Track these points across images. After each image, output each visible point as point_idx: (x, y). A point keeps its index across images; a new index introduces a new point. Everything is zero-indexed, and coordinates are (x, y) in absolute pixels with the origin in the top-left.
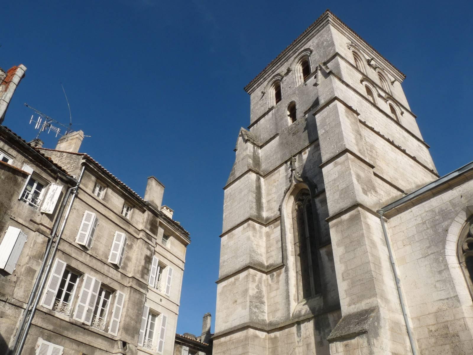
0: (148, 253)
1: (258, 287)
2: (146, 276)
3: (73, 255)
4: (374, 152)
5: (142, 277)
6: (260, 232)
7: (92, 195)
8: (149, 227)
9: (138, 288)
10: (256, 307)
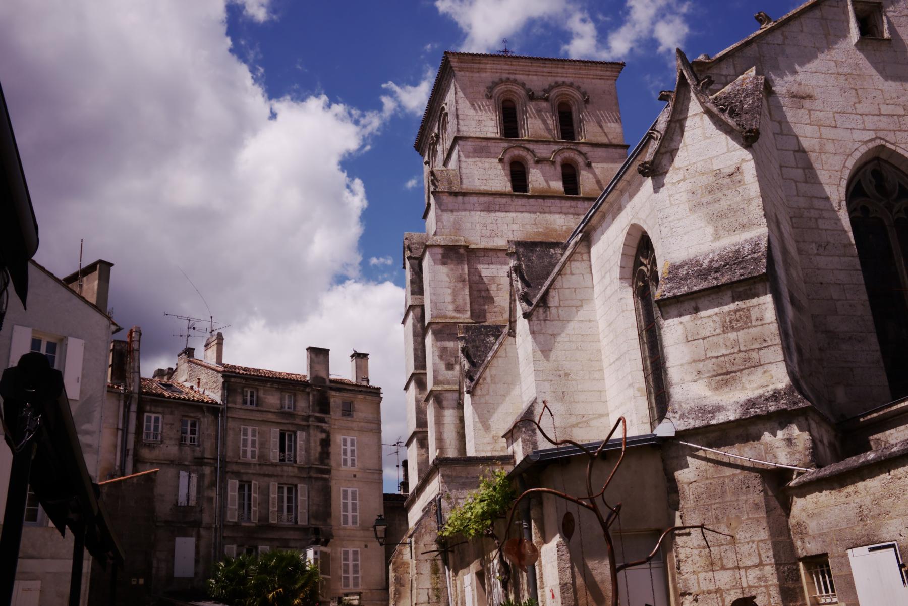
0: (324, 436)
2: (326, 461)
3: (242, 471)
5: (322, 463)
7: (244, 407)
8: (317, 408)
9: (320, 476)
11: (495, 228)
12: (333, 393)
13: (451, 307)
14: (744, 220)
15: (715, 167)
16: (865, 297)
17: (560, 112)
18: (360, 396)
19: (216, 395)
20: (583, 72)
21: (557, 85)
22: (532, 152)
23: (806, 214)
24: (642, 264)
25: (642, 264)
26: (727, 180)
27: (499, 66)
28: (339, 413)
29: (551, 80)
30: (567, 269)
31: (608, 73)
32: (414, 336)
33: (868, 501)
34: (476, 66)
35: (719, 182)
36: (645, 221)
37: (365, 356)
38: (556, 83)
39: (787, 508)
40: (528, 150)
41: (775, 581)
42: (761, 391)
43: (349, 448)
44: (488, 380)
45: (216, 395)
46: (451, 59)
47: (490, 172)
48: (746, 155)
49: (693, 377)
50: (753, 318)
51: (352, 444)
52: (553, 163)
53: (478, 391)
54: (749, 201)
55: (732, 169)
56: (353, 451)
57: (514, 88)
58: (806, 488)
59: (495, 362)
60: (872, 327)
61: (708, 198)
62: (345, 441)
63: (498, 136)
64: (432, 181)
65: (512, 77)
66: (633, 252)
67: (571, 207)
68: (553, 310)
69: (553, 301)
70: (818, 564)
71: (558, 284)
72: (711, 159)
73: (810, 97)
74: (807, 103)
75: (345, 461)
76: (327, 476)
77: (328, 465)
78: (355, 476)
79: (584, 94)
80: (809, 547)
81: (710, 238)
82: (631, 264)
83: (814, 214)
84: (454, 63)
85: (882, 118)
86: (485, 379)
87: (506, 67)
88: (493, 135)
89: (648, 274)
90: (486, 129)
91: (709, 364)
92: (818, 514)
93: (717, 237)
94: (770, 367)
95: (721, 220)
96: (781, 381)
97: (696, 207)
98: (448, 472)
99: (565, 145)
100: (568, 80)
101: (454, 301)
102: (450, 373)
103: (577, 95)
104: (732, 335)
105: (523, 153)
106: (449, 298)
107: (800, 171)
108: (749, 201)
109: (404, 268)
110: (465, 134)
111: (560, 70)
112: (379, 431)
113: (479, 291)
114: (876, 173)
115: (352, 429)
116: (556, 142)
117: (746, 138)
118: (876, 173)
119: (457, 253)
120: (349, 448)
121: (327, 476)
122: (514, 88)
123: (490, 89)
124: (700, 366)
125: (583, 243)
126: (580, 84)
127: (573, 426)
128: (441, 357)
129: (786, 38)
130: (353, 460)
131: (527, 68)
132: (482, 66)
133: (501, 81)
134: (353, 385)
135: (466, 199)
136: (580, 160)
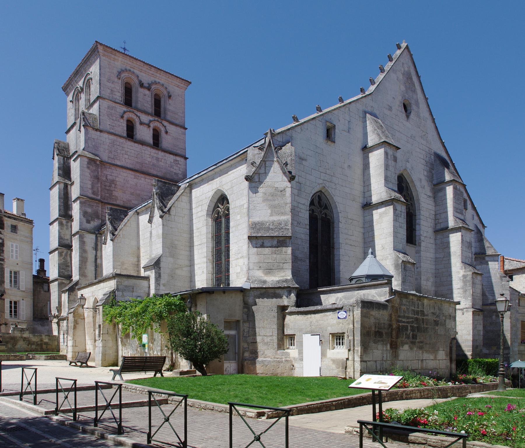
1: (64, 258)
4: (113, 185)
6: (67, 225)
10: (63, 269)
11: (116, 154)
12: (6, 219)
13: (90, 191)
14: (283, 211)
15: (276, 186)
16: (308, 245)
17: (155, 99)
18: (21, 223)
19: (257, 300)
20: (170, 80)
21: (156, 83)
22: (139, 117)
23: (296, 209)
24: (218, 207)
25: (218, 207)
26: (279, 193)
27: (126, 61)
28: (10, 230)
29: (152, 79)
30: (180, 199)
31: (182, 85)
32: (59, 198)
33: (314, 321)
34: (113, 56)
35: (276, 192)
36: (226, 190)
37: (22, 200)
38: (155, 82)
39: (284, 319)
40: (137, 116)
41: (276, 341)
42: (282, 278)
43: (14, 249)
44: (121, 236)
45: (257, 300)
46: (99, 46)
47: (116, 122)
48: (289, 185)
49: (258, 268)
50: (283, 251)
51: (16, 248)
52: (149, 126)
53: (116, 240)
54: (287, 204)
55: (282, 189)
56: (16, 251)
57: (133, 77)
58: (291, 313)
59: (125, 228)
60: (308, 257)
61: (270, 198)
62: (12, 246)
63: (122, 103)
64: (83, 118)
65: (132, 70)
66: (216, 201)
67: (155, 153)
68: (173, 217)
69: (173, 212)
70: (292, 337)
71: (175, 205)
72: (275, 182)
73: (306, 160)
74: (304, 162)
75: (12, 255)
76: (2, 262)
77: (3, 256)
78: (17, 264)
79: (169, 93)
80: (287, 332)
81: (269, 215)
82: (213, 206)
83: (299, 210)
84: (100, 48)
85: (327, 175)
86: (119, 235)
87: (129, 63)
88: (119, 101)
89: (222, 213)
90: (115, 97)
91: (265, 264)
92: (293, 322)
93: (271, 215)
94: (286, 270)
95: (275, 209)
96: (289, 276)
97: (264, 201)
98: (120, 280)
99: (156, 119)
100: (162, 82)
101: (92, 188)
102: (89, 225)
103: (165, 93)
104: (275, 256)
105: (135, 117)
106: (90, 186)
107: (297, 191)
108: (287, 204)
109: (53, 159)
110: (104, 96)
111: (158, 75)
112: (32, 243)
113: (105, 186)
114: (319, 197)
115: (16, 240)
116: (152, 115)
117: (291, 178)
118: (319, 197)
119: (95, 163)
120: (14, 249)
121: (2, 262)
122: (133, 77)
123: (120, 73)
124: (261, 265)
125: (188, 188)
126: (167, 87)
127: (176, 269)
128: (84, 216)
129: (302, 130)
130: (17, 256)
131: (141, 68)
132: (116, 58)
133: (126, 70)
134: (14, 215)
135: (102, 134)
136: (163, 129)
